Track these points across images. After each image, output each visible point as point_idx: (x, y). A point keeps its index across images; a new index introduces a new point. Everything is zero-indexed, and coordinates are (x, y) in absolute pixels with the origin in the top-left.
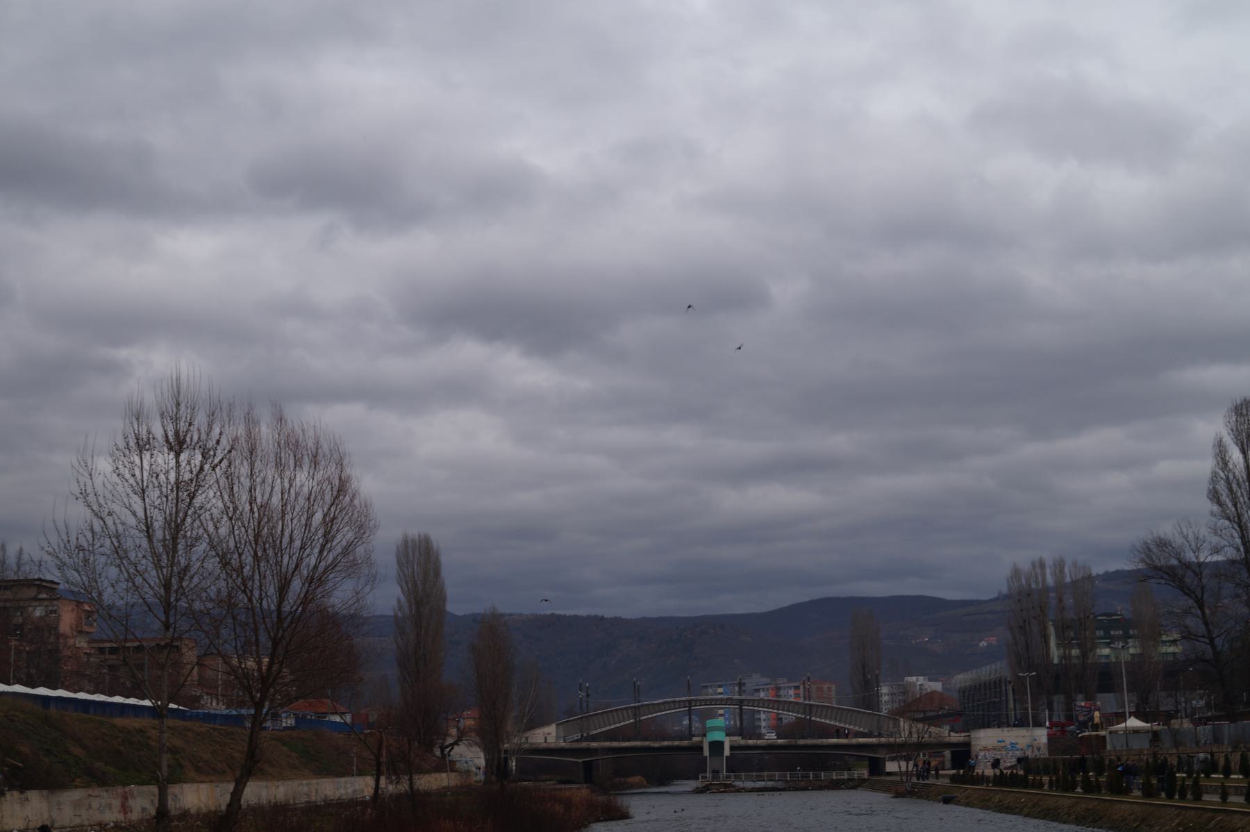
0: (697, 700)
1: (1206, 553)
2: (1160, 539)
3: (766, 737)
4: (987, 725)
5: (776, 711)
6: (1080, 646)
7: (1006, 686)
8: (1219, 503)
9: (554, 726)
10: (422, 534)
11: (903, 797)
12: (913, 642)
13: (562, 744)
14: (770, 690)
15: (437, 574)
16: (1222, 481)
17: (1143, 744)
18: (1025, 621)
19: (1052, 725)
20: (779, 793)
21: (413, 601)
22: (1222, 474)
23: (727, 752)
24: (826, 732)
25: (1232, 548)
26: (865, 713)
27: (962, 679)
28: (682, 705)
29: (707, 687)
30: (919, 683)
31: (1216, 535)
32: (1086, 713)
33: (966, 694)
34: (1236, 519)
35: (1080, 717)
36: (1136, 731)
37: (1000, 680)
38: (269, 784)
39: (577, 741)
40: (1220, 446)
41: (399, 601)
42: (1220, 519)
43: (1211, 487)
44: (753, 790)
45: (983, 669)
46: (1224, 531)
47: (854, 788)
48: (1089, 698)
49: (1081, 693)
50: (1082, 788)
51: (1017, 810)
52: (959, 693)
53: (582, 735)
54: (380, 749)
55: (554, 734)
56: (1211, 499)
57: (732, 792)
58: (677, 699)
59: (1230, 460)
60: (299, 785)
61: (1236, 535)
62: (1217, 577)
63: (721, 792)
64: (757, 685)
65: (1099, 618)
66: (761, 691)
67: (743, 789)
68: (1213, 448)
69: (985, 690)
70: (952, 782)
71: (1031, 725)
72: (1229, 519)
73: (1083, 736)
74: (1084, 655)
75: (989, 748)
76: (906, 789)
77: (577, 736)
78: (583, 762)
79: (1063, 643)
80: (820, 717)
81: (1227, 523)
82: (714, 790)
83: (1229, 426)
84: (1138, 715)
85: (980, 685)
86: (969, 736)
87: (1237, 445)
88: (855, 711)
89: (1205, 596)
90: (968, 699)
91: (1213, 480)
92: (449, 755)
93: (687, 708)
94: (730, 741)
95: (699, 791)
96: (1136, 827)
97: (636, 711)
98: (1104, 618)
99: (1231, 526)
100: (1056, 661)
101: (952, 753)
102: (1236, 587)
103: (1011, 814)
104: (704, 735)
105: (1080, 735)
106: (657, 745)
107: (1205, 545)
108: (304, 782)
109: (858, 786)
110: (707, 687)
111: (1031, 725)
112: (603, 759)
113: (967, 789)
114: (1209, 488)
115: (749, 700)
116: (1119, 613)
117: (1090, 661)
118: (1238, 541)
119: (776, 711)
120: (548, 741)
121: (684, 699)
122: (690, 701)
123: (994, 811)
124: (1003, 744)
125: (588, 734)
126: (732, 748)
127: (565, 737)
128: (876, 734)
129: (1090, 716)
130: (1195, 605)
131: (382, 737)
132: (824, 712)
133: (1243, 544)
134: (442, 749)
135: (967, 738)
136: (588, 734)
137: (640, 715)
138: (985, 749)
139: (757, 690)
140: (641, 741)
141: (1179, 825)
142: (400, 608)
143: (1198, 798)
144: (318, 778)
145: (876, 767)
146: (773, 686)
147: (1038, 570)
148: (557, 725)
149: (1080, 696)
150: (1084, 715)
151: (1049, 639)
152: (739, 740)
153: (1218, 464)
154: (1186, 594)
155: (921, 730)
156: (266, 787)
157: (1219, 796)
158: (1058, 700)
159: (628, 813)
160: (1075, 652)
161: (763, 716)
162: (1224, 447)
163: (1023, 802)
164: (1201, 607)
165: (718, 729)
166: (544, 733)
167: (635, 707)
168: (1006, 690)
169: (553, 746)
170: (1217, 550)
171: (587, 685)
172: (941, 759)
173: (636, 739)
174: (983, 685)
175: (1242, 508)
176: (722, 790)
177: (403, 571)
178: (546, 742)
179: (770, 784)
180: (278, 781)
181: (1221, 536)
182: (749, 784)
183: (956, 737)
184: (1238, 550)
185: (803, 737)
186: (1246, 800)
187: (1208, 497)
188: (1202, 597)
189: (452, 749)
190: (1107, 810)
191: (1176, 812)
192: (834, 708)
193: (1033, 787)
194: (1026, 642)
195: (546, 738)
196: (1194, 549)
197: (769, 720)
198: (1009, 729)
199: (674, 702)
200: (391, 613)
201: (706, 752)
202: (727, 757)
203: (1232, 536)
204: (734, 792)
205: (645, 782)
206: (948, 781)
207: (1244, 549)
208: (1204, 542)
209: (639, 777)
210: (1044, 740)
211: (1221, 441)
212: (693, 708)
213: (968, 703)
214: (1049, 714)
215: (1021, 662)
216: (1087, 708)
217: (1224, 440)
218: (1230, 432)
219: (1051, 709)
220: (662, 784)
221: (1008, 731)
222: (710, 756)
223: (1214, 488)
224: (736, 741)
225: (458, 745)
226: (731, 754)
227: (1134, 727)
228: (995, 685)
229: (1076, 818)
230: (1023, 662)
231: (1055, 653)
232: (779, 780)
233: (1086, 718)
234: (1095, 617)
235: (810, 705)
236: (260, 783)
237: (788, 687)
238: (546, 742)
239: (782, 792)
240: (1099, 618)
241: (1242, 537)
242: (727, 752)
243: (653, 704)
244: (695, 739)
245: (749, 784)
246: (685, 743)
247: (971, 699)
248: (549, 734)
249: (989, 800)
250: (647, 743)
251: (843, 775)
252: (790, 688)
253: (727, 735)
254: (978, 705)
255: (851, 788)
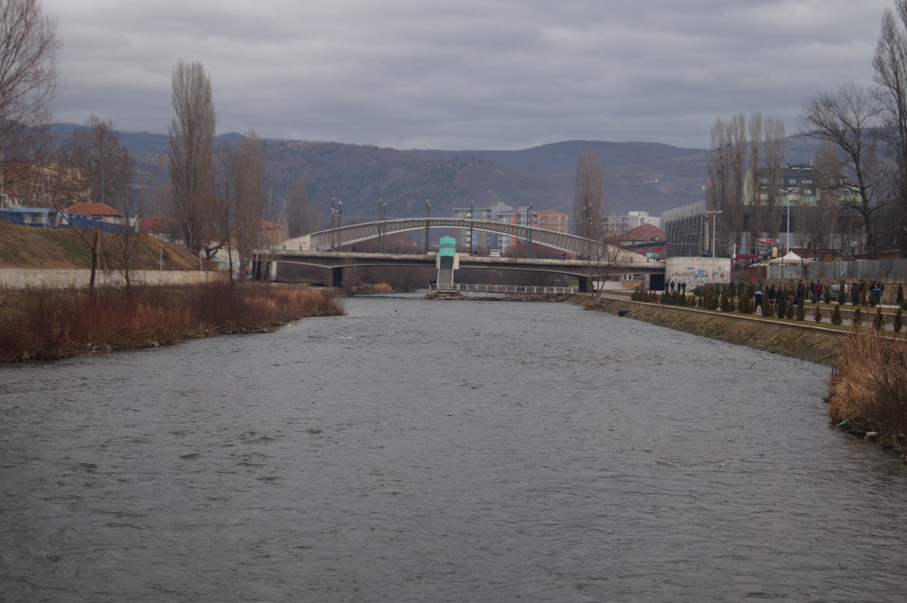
0: (433, 221)
1: (865, 114)
2: (827, 99)
3: (491, 255)
4: (683, 254)
5: (514, 236)
6: (768, 191)
7: (704, 223)
8: (882, 70)
9: (309, 236)
10: (195, 62)
11: (592, 310)
12: (645, 182)
13: (315, 253)
14: (512, 217)
15: (208, 100)
16: (887, 52)
17: (790, 274)
18: (723, 167)
19: (738, 257)
20: (498, 302)
21: (186, 122)
22: (887, 46)
23: (456, 266)
24: (547, 253)
25: (889, 111)
26: (577, 238)
27: (672, 214)
28: (420, 224)
29: (458, 211)
30: (641, 217)
31: (876, 99)
32: (767, 248)
33: (672, 227)
34: (895, 86)
35: (760, 252)
36: (794, 264)
37: (699, 217)
38: (27, 271)
39: (329, 250)
40: (888, 20)
41: (173, 122)
42: (881, 85)
43: (876, 56)
44: (474, 299)
45: (687, 207)
46: (884, 96)
47: (562, 301)
48: (772, 235)
49: (766, 231)
50: (721, 307)
51: (668, 323)
52: (666, 226)
53: (333, 246)
54: (95, 242)
55: (308, 244)
56: (876, 67)
57: (456, 299)
58: (416, 219)
59: (896, 33)
60: (57, 273)
61: (894, 99)
62: (873, 135)
63: (447, 299)
64: (501, 212)
65: (793, 168)
66: (504, 217)
67: (466, 297)
68: (882, 22)
69: (687, 225)
70: (633, 299)
71: (714, 256)
72: (889, 85)
73: (753, 267)
74: (771, 200)
75: (680, 273)
76: (596, 304)
77: (328, 247)
78: (333, 268)
79: (757, 187)
80: (538, 240)
81: (887, 88)
82: (442, 298)
83: (899, 3)
84: (796, 251)
85: (683, 221)
86: (665, 262)
87: (904, 20)
88: (571, 237)
89: (862, 151)
90: (673, 231)
91: (879, 50)
92: (214, 257)
93: (425, 227)
94: (460, 257)
95: (430, 298)
96: (746, 340)
97: (382, 227)
98: (798, 168)
99: (890, 92)
100: (746, 203)
101: (652, 276)
102: (889, 144)
103: (663, 326)
104: (438, 251)
105: (751, 266)
106: (396, 257)
107: (865, 106)
108: (63, 271)
109: (565, 300)
110: (458, 211)
111: (714, 256)
112: (349, 267)
113: (639, 305)
114: (875, 57)
115: (478, 223)
116: (811, 165)
117: (775, 204)
118: (896, 105)
119: (514, 236)
120: (303, 249)
121: (422, 219)
122: (428, 222)
123: (652, 324)
124: (691, 271)
125: (339, 244)
126: (461, 263)
127: (317, 247)
128: (586, 256)
129: (769, 251)
130: (852, 158)
131: (97, 233)
132: (582, 244)
133: (899, 108)
134: (208, 251)
135: (663, 265)
136: (339, 244)
137: (384, 231)
138: (677, 274)
139: (501, 217)
140: (383, 253)
141: (775, 339)
142: (175, 127)
143: (801, 318)
144: (75, 269)
145: (584, 285)
146: (515, 214)
147: (738, 124)
148: (312, 236)
149: (765, 234)
150: (765, 250)
151: (743, 183)
152: (467, 257)
153: (885, 36)
154: (845, 148)
155: (611, 254)
156: (25, 274)
157: (814, 317)
158: (745, 236)
159: (342, 311)
160: (764, 197)
161: (504, 239)
162: (892, 21)
163: (675, 317)
164: (857, 161)
165: (447, 247)
166: (300, 242)
167: (380, 224)
168: (703, 225)
169: (307, 254)
170: (875, 112)
171: (340, 203)
172: (642, 281)
173: (379, 251)
174: (685, 221)
175: (902, 76)
176: (448, 297)
177: (178, 96)
178: (301, 250)
179: (490, 295)
180: (36, 269)
181: (880, 99)
182: (472, 294)
183: (653, 263)
184: (895, 113)
185: (525, 257)
186: (832, 321)
187: (873, 65)
188: (858, 152)
189: (216, 251)
190: (730, 326)
191: (777, 329)
192: (559, 234)
193: (688, 305)
194: (723, 186)
195: (301, 247)
196: (855, 110)
197: (509, 242)
198: (698, 258)
199: (414, 221)
200: (167, 133)
201: (438, 265)
202: (455, 270)
203: (891, 101)
204: (458, 300)
205: (390, 289)
206: (630, 298)
207: (900, 112)
208: (865, 104)
209: (384, 284)
210: (728, 269)
211: (889, 16)
212: (431, 227)
213: (673, 235)
214: (737, 248)
215: (716, 202)
216: (768, 244)
217: (892, 15)
218: (899, 8)
219: (739, 243)
220: (406, 291)
221: (697, 260)
222: (441, 269)
223: (879, 57)
224: (464, 257)
225: (221, 248)
226: (460, 268)
227: (790, 260)
228: (696, 221)
229: (707, 331)
230: (718, 203)
231: (747, 200)
232: (508, 293)
233: (765, 252)
234: (790, 167)
235: (531, 230)
236: (19, 270)
237: (481, 210)
238: (301, 250)
239: (500, 302)
240: (793, 168)
241: (899, 102)
242: (456, 266)
243: (395, 223)
244: (430, 254)
245: (472, 294)
246: (421, 257)
247: (675, 232)
248: (304, 243)
249: (652, 315)
250: (388, 255)
251: (553, 290)
252: (484, 210)
253: (457, 251)
254: (680, 238)
255: (559, 302)
